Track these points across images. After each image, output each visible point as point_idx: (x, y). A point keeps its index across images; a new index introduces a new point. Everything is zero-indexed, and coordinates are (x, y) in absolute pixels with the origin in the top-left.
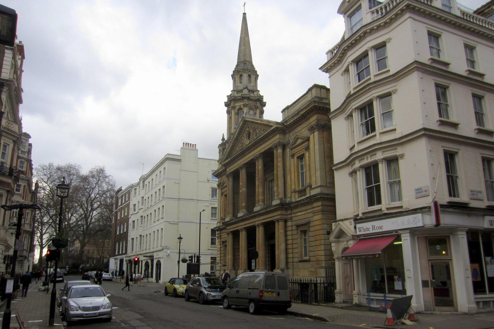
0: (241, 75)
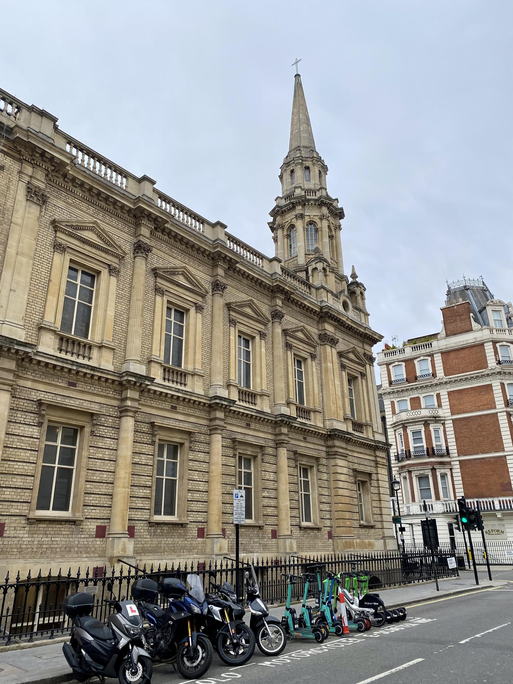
0: (292, 171)
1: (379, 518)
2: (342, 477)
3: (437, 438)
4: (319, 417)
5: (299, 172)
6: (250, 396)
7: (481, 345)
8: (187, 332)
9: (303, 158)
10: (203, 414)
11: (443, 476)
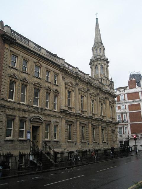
0: (96, 49)
1: (116, 140)
2: (110, 131)
3: (125, 118)
4: (74, 109)
5: (98, 51)
6: (70, 108)
7: (138, 92)
8: (71, 97)
9: (99, 46)
10: (75, 117)
11: (126, 128)
